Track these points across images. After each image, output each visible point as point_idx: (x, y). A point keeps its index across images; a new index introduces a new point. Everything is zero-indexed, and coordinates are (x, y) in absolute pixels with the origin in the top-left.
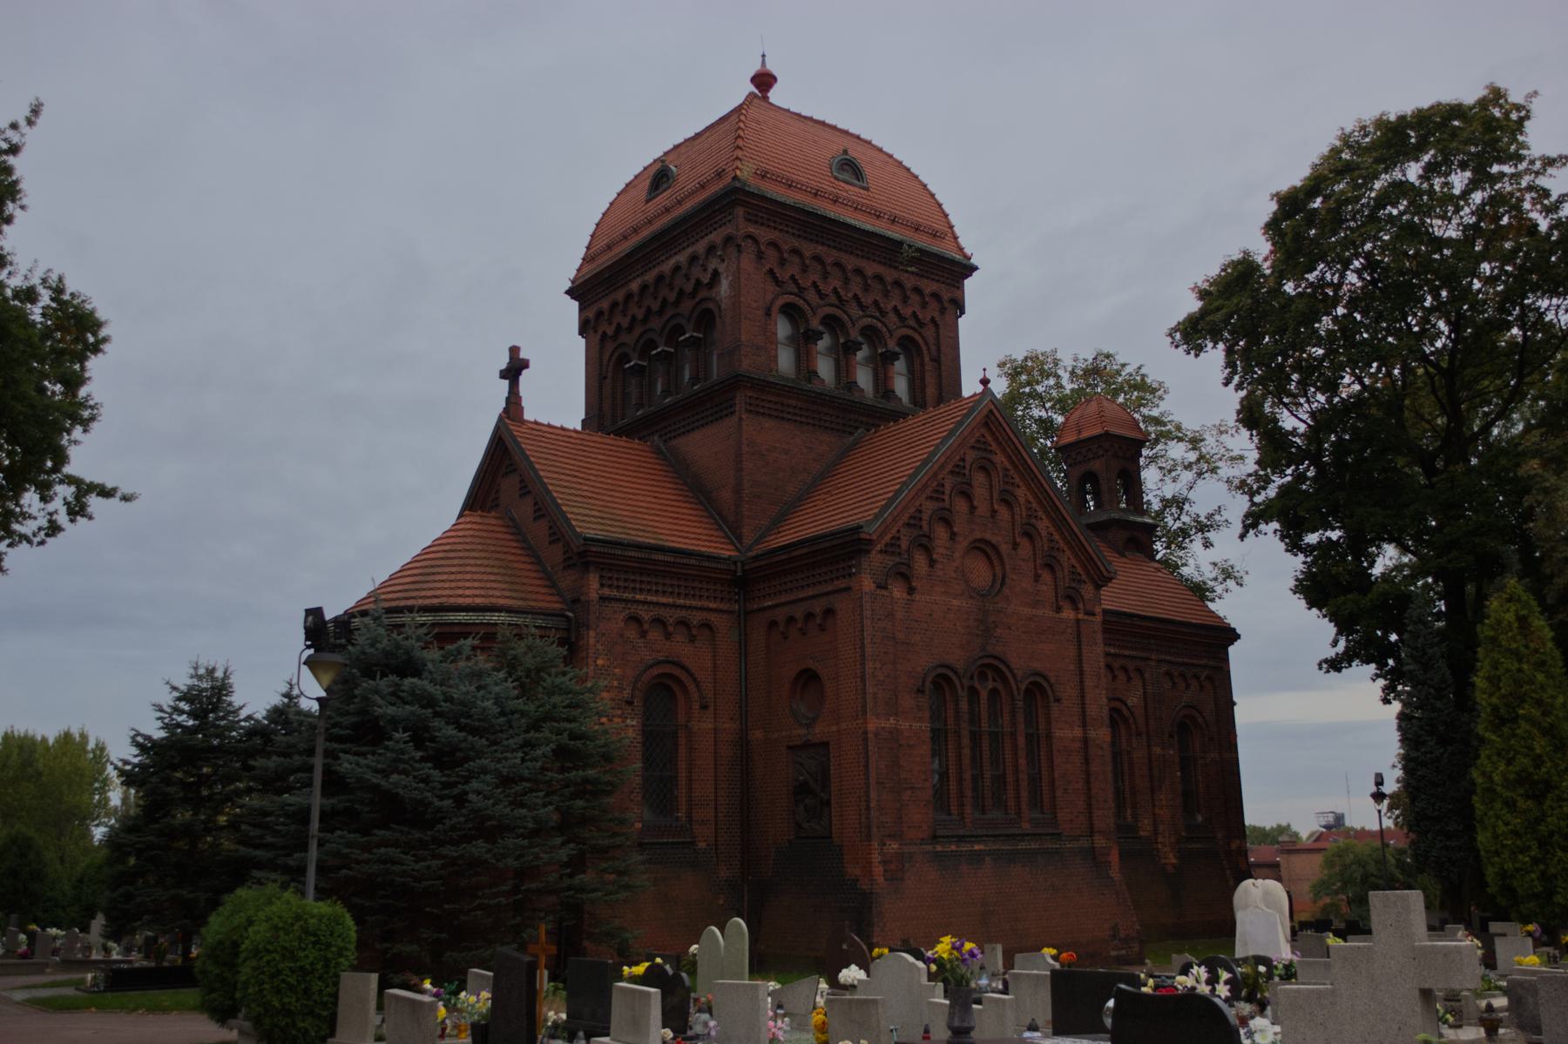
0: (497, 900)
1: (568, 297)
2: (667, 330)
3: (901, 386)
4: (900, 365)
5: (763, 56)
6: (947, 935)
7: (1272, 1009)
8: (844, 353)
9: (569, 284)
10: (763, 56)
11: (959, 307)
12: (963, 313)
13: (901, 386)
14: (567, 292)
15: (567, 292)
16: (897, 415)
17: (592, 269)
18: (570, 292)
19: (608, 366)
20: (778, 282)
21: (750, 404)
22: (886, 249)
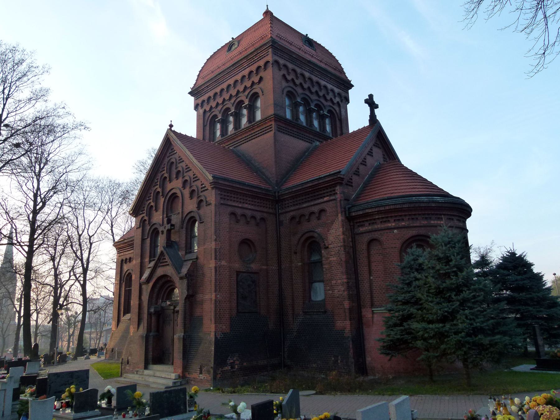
0: (176, 341)
1: (190, 95)
2: (249, 96)
3: (328, 128)
4: (327, 121)
5: (267, 6)
6: (117, 404)
7: (406, 399)
8: (309, 113)
9: (190, 90)
10: (267, 6)
11: (347, 100)
12: (349, 102)
13: (328, 128)
14: (190, 93)
15: (190, 93)
16: (326, 138)
17: (201, 82)
18: (190, 93)
19: (207, 121)
20: (287, 81)
21: (279, 128)
22: (324, 73)
